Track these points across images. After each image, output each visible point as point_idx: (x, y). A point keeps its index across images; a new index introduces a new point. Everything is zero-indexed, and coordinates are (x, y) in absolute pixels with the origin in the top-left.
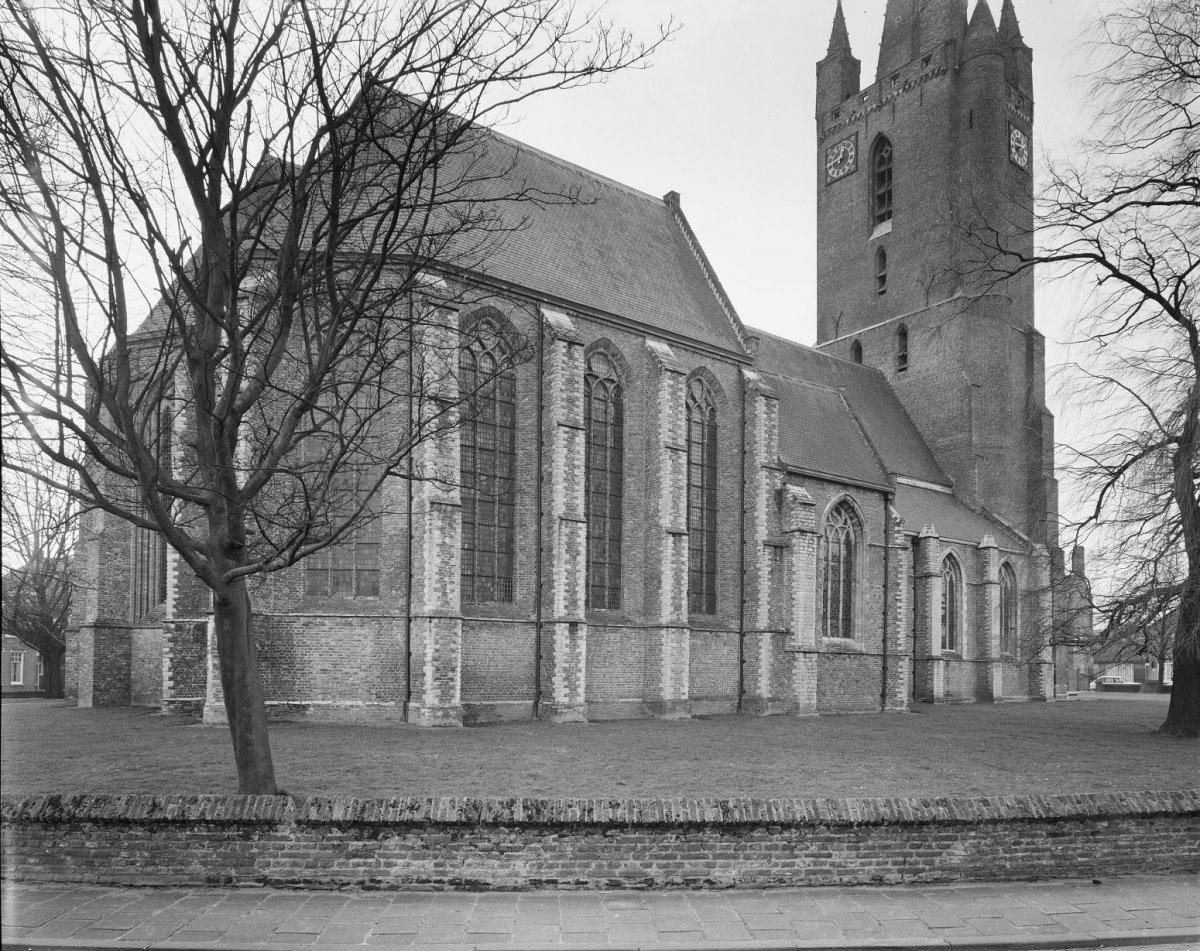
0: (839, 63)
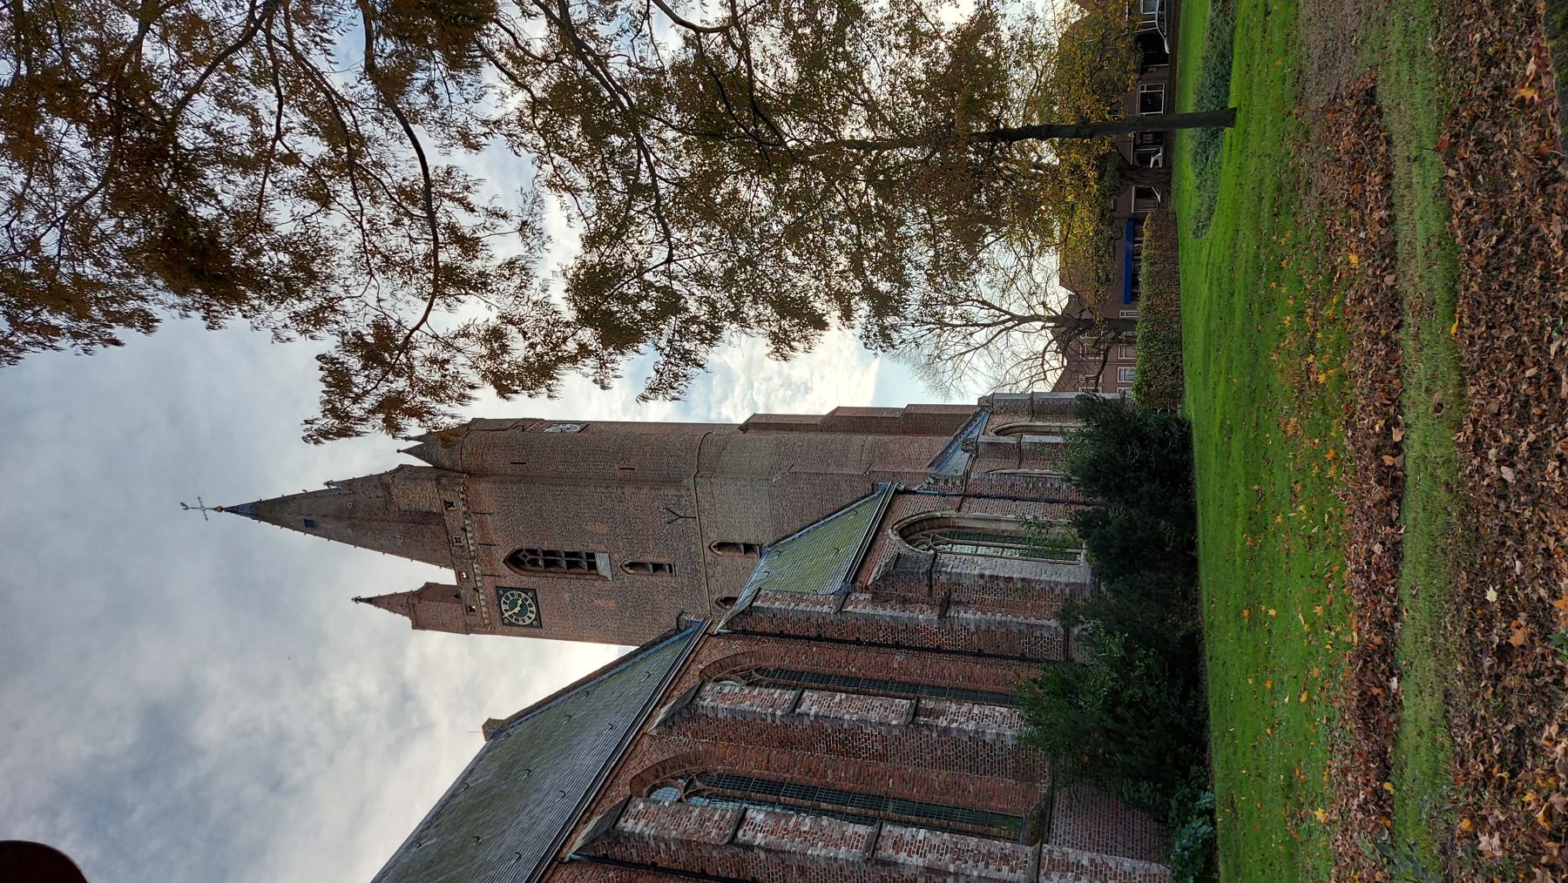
0: (420, 608)
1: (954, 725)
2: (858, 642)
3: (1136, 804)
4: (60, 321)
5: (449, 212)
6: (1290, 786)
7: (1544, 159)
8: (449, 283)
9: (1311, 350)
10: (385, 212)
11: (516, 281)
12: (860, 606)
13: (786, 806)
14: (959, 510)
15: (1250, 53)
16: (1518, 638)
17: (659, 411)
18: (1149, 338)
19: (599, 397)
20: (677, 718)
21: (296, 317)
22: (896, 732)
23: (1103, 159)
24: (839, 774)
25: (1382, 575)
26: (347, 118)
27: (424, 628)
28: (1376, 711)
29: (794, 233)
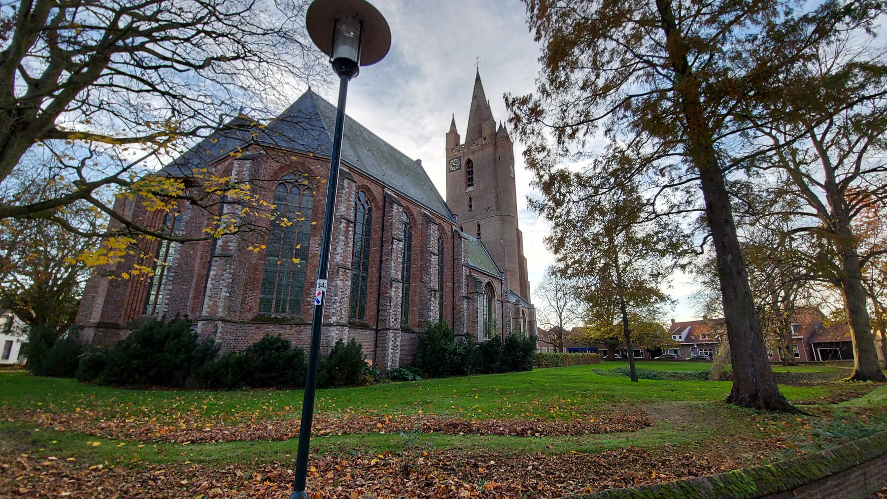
0: (453, 135)
3: (415, 359)
4: (536, 11)
5: (583, 128)
6: (427, 403)
7: (633, 480)
8: (560, 131)
9: (561, 408)
10: (581, 108)
11: (562, 153)
12: (465, 272)
15: (657, 385)
16: (480, 470)
17: (521, 204)
18: (557, 357)
19: (525, 182)
21: (543, 85)
23: (617, 339)
24: (414, 270)
25: (493, 430)
26: (612, 91)
28: (453, 428)
29: (586, 241)
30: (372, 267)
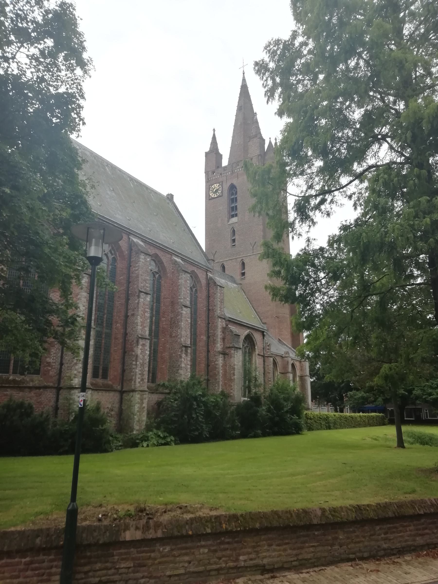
0: (213, 154)
1: (183, 360)
2: (209, 323)
12: (220, 324)
13: (153, 306)
14: (259, 355)
20: (177, 266)
22: (179, 340)
27: (206, 156)
30: (117, 322)
